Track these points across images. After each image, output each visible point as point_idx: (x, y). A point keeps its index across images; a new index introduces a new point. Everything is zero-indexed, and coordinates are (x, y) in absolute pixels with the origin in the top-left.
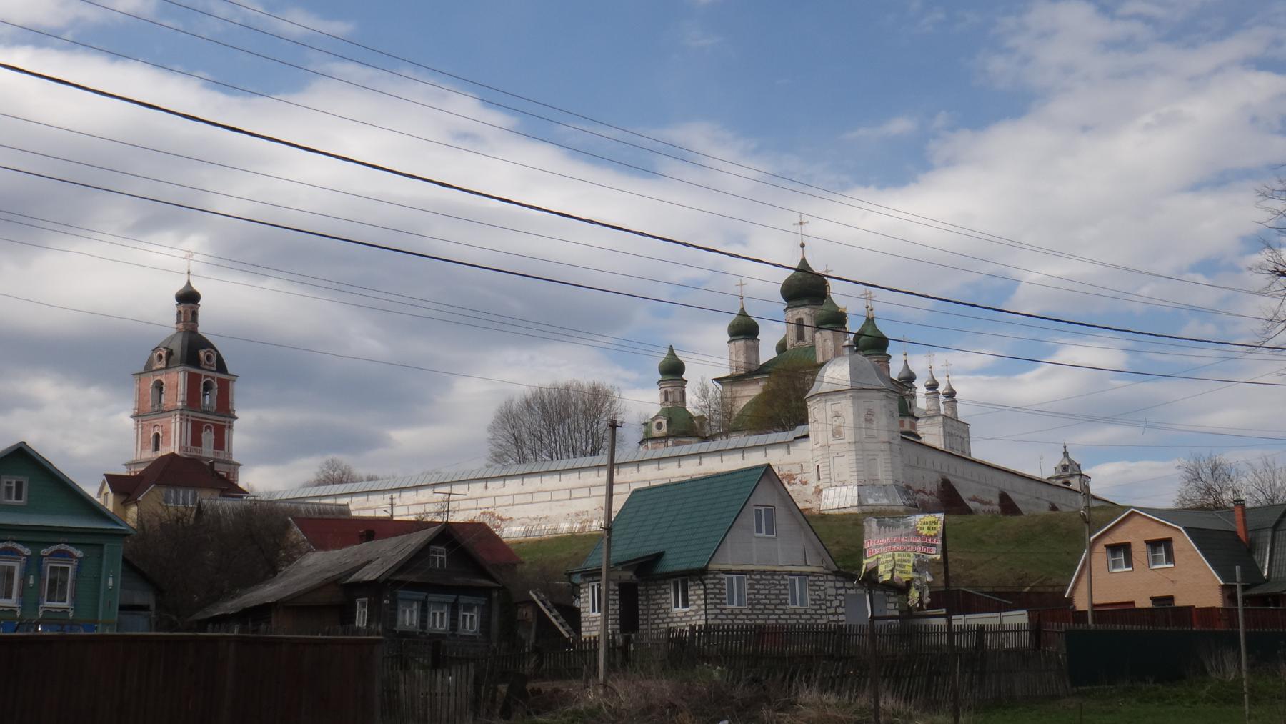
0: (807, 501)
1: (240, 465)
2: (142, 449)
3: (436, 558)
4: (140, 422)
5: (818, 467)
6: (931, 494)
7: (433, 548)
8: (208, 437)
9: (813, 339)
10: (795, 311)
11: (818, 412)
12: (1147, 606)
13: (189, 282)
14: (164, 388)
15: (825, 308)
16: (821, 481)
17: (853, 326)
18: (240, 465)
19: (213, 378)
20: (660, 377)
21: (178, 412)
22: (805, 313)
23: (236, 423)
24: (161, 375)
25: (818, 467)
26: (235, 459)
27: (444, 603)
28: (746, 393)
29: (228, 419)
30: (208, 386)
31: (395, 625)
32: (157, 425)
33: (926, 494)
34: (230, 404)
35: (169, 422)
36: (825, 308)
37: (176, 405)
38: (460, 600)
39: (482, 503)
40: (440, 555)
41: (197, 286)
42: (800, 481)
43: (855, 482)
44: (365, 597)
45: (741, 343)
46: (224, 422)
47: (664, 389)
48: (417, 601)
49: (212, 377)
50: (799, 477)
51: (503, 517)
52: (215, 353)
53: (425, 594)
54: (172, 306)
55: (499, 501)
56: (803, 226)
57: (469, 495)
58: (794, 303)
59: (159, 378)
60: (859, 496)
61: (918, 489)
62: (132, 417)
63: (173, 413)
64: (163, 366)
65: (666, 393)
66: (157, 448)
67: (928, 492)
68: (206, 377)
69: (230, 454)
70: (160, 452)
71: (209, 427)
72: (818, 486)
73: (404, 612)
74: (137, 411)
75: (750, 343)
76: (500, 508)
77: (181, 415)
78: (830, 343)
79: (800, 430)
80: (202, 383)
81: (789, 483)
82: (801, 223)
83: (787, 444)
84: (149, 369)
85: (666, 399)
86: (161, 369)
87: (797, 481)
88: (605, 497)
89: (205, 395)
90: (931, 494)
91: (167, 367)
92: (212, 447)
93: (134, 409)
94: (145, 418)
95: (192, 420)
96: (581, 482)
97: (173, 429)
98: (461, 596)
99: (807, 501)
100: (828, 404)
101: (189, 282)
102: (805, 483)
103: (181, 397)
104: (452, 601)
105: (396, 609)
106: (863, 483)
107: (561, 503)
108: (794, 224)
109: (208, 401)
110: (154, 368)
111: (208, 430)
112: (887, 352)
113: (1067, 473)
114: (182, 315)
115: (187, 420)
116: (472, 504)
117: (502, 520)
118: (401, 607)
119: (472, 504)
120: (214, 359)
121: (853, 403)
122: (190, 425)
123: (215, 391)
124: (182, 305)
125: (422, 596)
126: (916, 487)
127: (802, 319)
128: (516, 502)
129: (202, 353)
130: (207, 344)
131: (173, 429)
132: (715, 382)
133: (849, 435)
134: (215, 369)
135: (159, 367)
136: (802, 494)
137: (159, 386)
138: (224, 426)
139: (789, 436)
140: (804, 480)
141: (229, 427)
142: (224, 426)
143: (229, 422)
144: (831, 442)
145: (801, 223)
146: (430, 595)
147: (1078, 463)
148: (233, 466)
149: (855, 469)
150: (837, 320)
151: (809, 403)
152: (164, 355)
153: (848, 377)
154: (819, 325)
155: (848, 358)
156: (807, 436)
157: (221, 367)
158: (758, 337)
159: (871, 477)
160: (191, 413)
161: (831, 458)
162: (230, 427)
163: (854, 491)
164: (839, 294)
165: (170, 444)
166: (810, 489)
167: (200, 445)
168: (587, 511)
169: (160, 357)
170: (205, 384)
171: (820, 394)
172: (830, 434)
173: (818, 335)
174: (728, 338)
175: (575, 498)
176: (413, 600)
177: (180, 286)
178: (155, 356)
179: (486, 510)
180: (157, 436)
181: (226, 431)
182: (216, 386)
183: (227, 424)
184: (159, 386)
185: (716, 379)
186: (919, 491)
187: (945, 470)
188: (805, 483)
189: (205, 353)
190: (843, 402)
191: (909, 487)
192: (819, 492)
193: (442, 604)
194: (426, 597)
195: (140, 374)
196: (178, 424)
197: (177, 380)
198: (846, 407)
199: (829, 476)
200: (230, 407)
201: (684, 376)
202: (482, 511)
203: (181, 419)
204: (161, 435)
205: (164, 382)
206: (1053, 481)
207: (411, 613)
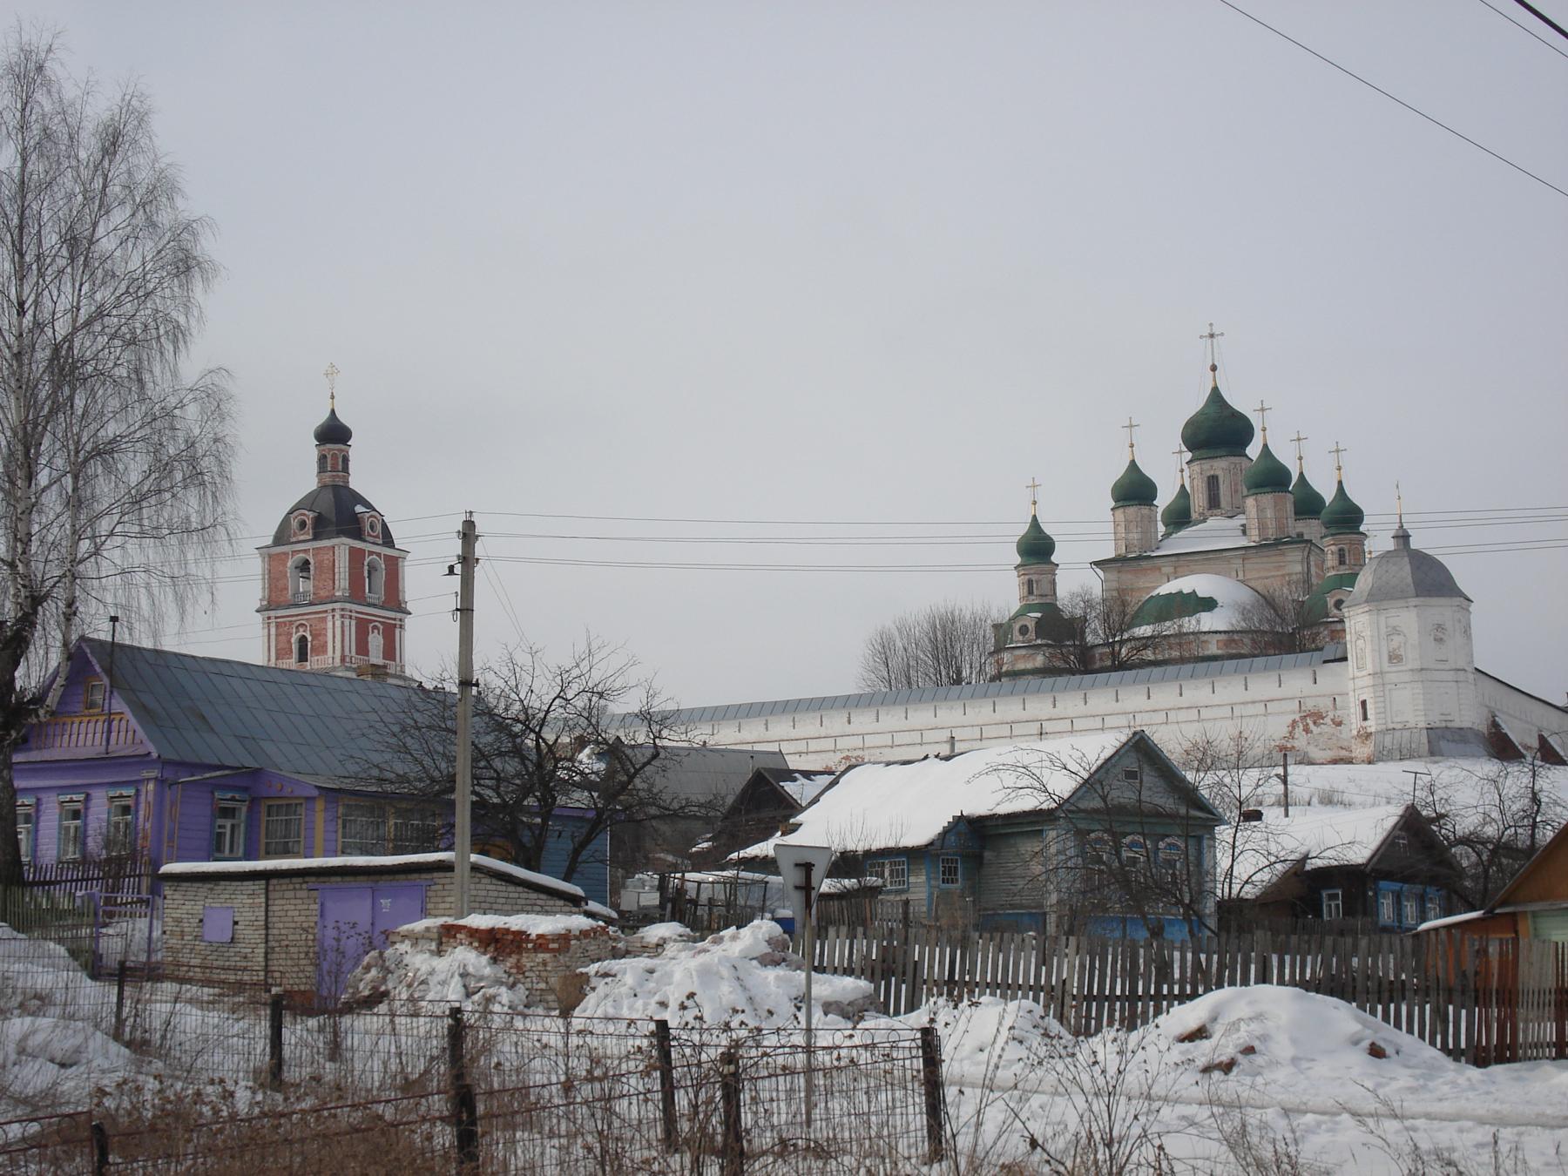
0: (1342, 748)
8: (376, 641)
10: (1206, 465)
13: (333, 411)
19: (379, 555)
20: (1018, 560)
23: (408, 621)
29: (399, 615)
34: (401, 594)
37: (334, 595)
39: (843, 743)
42: (1332, 720)
44: (1321, 895)
45: (1132, 510)
46: (395, 619)
47: (1027, 577)
50: (1331, 715)
54: (310, 451)
55: (869, 741)
56: (1215, 340)
57: (823, 732)
58: (1203, 452)
60: (1429, 742)
62: (257, 611)
65: (1030, 582)
68: (371, 553)
70: (308, 663)
71: (375, 627)
73: (1389, 918)
74: (265, 603)
75: (1145, 510)
76: (872, 751)
80: (366, 563)
81: (1315, 723)
82: (1212, 336)
85: (1030, 592)
87: (1328, 720)
92: (381, 655)
93: (261, 600)
96: (998, 717)
99: (1342, 748)
101: (333, 411)
102: (1340, 724)
106: (1433, 725)
108: (1201, 337)
111: (376, 631)
114: (329, 461)
116: (828, 744)
119: (828, 744)
120: (379, 528)
121: (1418, 616)
122: (353, 622)
127: (1217, 477)
128: (866, 746)
132: (1098, 570)
134: (381, 542)
136: (1334, 738)
140: (1337, 720)
141: (401, 627)
143: (401, 620)
145: (1212, 336)
149: (1422, 707)
152: (309, 522)
157: (388, 540)
158: (1155, 502)
159: (1443, 718)
160: (355, 607)
161: (1387, 692)
165: (325, 652)
169: (303, 525)
172: (1385, 658)
174: (1113, 504)
178: (295, 524)
180: (303, 640)
181: (397, 631)
182: (383, 566)
185: (1097, 563)
187: (1493, 705)
200: (401, 598)
201: (1054, 558)
202: (844, 755)
204: (309, 639)
205: (312, 561)
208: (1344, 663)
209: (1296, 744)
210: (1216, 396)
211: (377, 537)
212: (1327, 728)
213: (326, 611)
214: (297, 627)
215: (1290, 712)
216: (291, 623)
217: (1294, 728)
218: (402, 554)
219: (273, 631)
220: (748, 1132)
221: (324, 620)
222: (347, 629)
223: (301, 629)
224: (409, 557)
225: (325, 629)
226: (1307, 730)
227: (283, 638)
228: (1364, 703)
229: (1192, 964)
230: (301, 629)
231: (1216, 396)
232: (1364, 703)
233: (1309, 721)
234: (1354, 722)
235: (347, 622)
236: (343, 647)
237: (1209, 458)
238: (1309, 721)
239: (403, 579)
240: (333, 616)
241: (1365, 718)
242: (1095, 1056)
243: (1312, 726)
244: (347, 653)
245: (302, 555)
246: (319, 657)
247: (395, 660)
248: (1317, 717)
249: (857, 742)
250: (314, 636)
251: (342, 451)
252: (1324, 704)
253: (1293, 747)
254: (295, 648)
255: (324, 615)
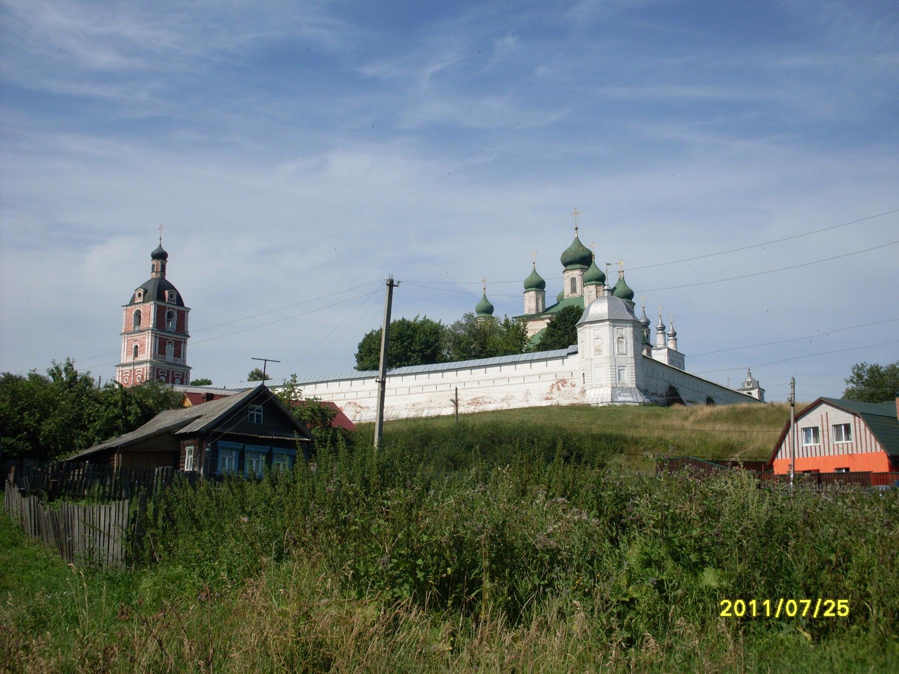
1: (191, 368)
2: (127, 356)
3: (254, 414)
4: (126, 338)
5: (584, 374)
6: (661, 396)
7: (251, 406)
8: (170, 349)
9: (582, 291)
11: (584, 334)
12: (880, 471)
14: (142, 316)
15: (591, 272)
16: (585, 384)
17: (611, 282)
18: (191, 368)
19: (174, 309)
21: (150, 332)
22: (576, 273)
23: (189, 340)
24: (140, 307)
25: (584, 374)
26: (188, 364)
27: (233, 449)
28: (536, 327)
29: (183, 337)
30: (170, 315)
31: (215, 470)
32: (136, 340)
33: (658, 396)
35: (144, 338)
36: (591, 272)
38: (273, 450)
39: (348, 396)
40: (257, 410)
41: (165, 249)
43: (610, 385)
48: (236, 450)
49: (173, 309)
50: (570, 381)
51: (363, 406)
52: (176, 293)
53: (243, 444)
54: (149, 262)
55: (360, 395)
58: (570, 267)
59: (138, 309)
60: (611, 394)
61: (653, 392)
63: (147, 332)
64: (141, 301)
66: (136, 355)
67: (659, 395)
68: (169, 308)
69: (184, 361)
71: (169, 342)
72: (583, 387)
77: (152, 333)
78: (594, 293)
79: (571, 348)
80: (166, 313)
81: (562, 385)
83: (563, 358)
84: (132, 303)
86: (140, 303)
87: (568, 384)
88: (449, 411)
89: (168, 321)
90: (661, 396)
91: (144, 302)
94: (129, 336)
95: (159, 337)
97: (147, 343)
98: (275, 448)
100: (592, 330)
102: (574, 386)
103: (152, 322)
104: (267, 451)
105: (217, 457)
107: (403, 397)
109: (171, 325)
110: (136, 302)
112: (633, 301)
113: (749, 387)
115: (156, 337)
117: (361, 408)
118: (221, 454)
120: (175, 297)
123: (175, 318)
124: (155, 260)
125: (240, 446)
126: (652, 391)
129: (167, 293)
130: (171, 287)
131: (147, 343)
133: (606, 352)
134: (175, 303)
135: (139, 301)
137: (138, 315)
138: (181, 342)
139: (564, 352)
140: (573, 384)
141: (184, 342)
142: (181, 342)
144: (593, 356)
146: (246, 445)
147: (757, 380)
148: (186, 369)
150: (600, 279)
151: (578, 329)
152: (142, 294)
153: (607, 311)
154: (586, 282)
155: (606, 300)
156: (576, 353)
157: (180, 301)
161: (593, 368)
162: (185, 343)
163: (608, 391)
164: (600, 262)
165: (144, 353)
166: (577, 390)
167: (164, 353)
168: (420, 403)
169: (140, 295)
170: (168, 313)
171: (587, 323)
172: (593, 351)
173: (585, 289)
175: (412, 394)
176: (233, 449)
177: (154, 248)
178: (137, 295)
179: (351, 401)
180: (136, 347)
181: (182, 345)
182: (176, 315)
183: (183, 341)
184: (138, 315)
186: (653, 394)
187: (671, 380)
188: (574, 386)
189: (169, 293)
190: (603, 328)
191: (646, 391)
192: (584, 392)
193: (258, 454)
194: (244, 447)
195: (127, 306)
196: (150, 339)
197: (149, 310)
198: (605, 330)
199: (591, 380)
202: (348, 401)
203: (152, 336)
205: (142, 311)
206: (741, 392)
207: (230, 460)
208: (577, 355)
209: (553, 396)
210: (577, 241)
211: (174, 301)
212: (568, 388)
215: (551, 380)
217: (552, 388)
218: (187, 310)
220: (473, 622)
225: (145, 342)
226: (559, 389)
231: (577, 241)
233: (560, 384)
237: (571, 270)
238: (560, 384)
239: (187, 321)
243: (561, 386)
247: (180, 358)
248: (564, 382)
249: (354, 395)
250: (141, 345)
252: (567, 376)
253: (552, 398)
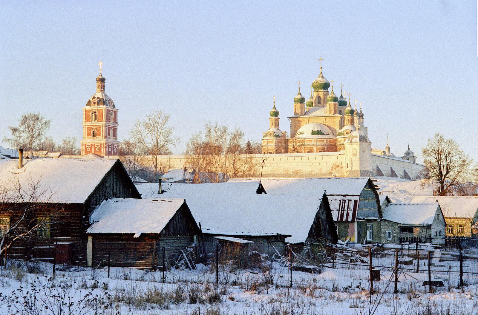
19: (112, 111)
23: (118, 127)
46: (115, 127)
71: (112, 129)
81: (337, 167)
87: (340, 167)
102: (342, 168)
122: (107, 128)
132: (290, 119)
145: (321, 59)
204: (96, 131)
211: (112, 106)
212: (339, 169)
213: (101, 125)
214: (93, 128)
216: (91, 127)
219: (86, 129)
221: (100, 127)
222: (106, 129)
223: (94, 129)
224: (119, 111)
226: (335, 169)
227: (89, 131)
228: (347, 164)
229: (248, 240)
230: (94, 129)
232: (347, 164)
234: (345, 168)
235: (106, 128)
236: (105, 135)
240: (103, 126)
241: (347, 167)
242: (103, 88)
243: (336, 168)
244: (106, 136)
245: (94, 111)
246: (99, 136)
248: (338, 166)
250: (97, 131)
251: (103, 84)
254: (92, 133)
255: (100, 126)
